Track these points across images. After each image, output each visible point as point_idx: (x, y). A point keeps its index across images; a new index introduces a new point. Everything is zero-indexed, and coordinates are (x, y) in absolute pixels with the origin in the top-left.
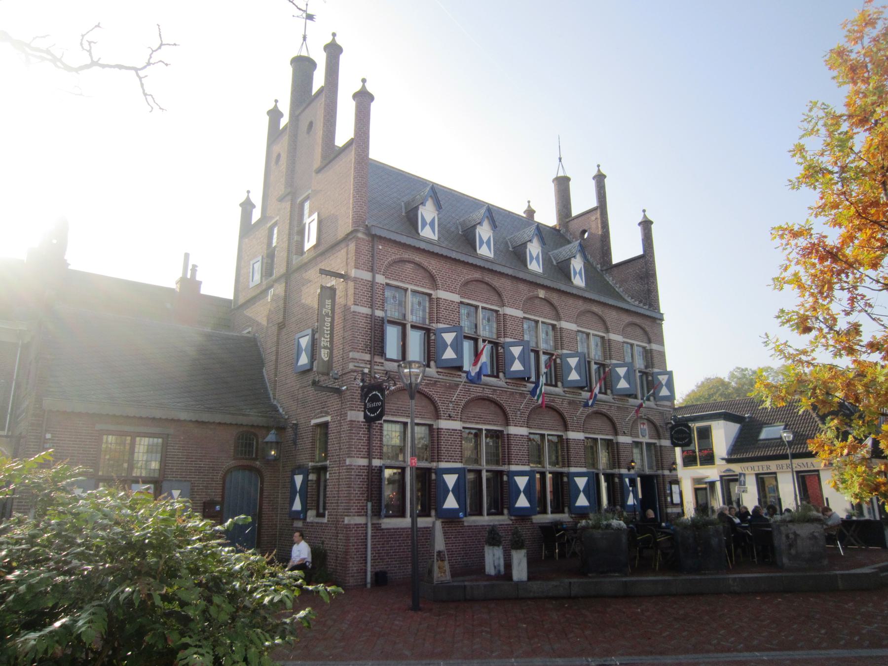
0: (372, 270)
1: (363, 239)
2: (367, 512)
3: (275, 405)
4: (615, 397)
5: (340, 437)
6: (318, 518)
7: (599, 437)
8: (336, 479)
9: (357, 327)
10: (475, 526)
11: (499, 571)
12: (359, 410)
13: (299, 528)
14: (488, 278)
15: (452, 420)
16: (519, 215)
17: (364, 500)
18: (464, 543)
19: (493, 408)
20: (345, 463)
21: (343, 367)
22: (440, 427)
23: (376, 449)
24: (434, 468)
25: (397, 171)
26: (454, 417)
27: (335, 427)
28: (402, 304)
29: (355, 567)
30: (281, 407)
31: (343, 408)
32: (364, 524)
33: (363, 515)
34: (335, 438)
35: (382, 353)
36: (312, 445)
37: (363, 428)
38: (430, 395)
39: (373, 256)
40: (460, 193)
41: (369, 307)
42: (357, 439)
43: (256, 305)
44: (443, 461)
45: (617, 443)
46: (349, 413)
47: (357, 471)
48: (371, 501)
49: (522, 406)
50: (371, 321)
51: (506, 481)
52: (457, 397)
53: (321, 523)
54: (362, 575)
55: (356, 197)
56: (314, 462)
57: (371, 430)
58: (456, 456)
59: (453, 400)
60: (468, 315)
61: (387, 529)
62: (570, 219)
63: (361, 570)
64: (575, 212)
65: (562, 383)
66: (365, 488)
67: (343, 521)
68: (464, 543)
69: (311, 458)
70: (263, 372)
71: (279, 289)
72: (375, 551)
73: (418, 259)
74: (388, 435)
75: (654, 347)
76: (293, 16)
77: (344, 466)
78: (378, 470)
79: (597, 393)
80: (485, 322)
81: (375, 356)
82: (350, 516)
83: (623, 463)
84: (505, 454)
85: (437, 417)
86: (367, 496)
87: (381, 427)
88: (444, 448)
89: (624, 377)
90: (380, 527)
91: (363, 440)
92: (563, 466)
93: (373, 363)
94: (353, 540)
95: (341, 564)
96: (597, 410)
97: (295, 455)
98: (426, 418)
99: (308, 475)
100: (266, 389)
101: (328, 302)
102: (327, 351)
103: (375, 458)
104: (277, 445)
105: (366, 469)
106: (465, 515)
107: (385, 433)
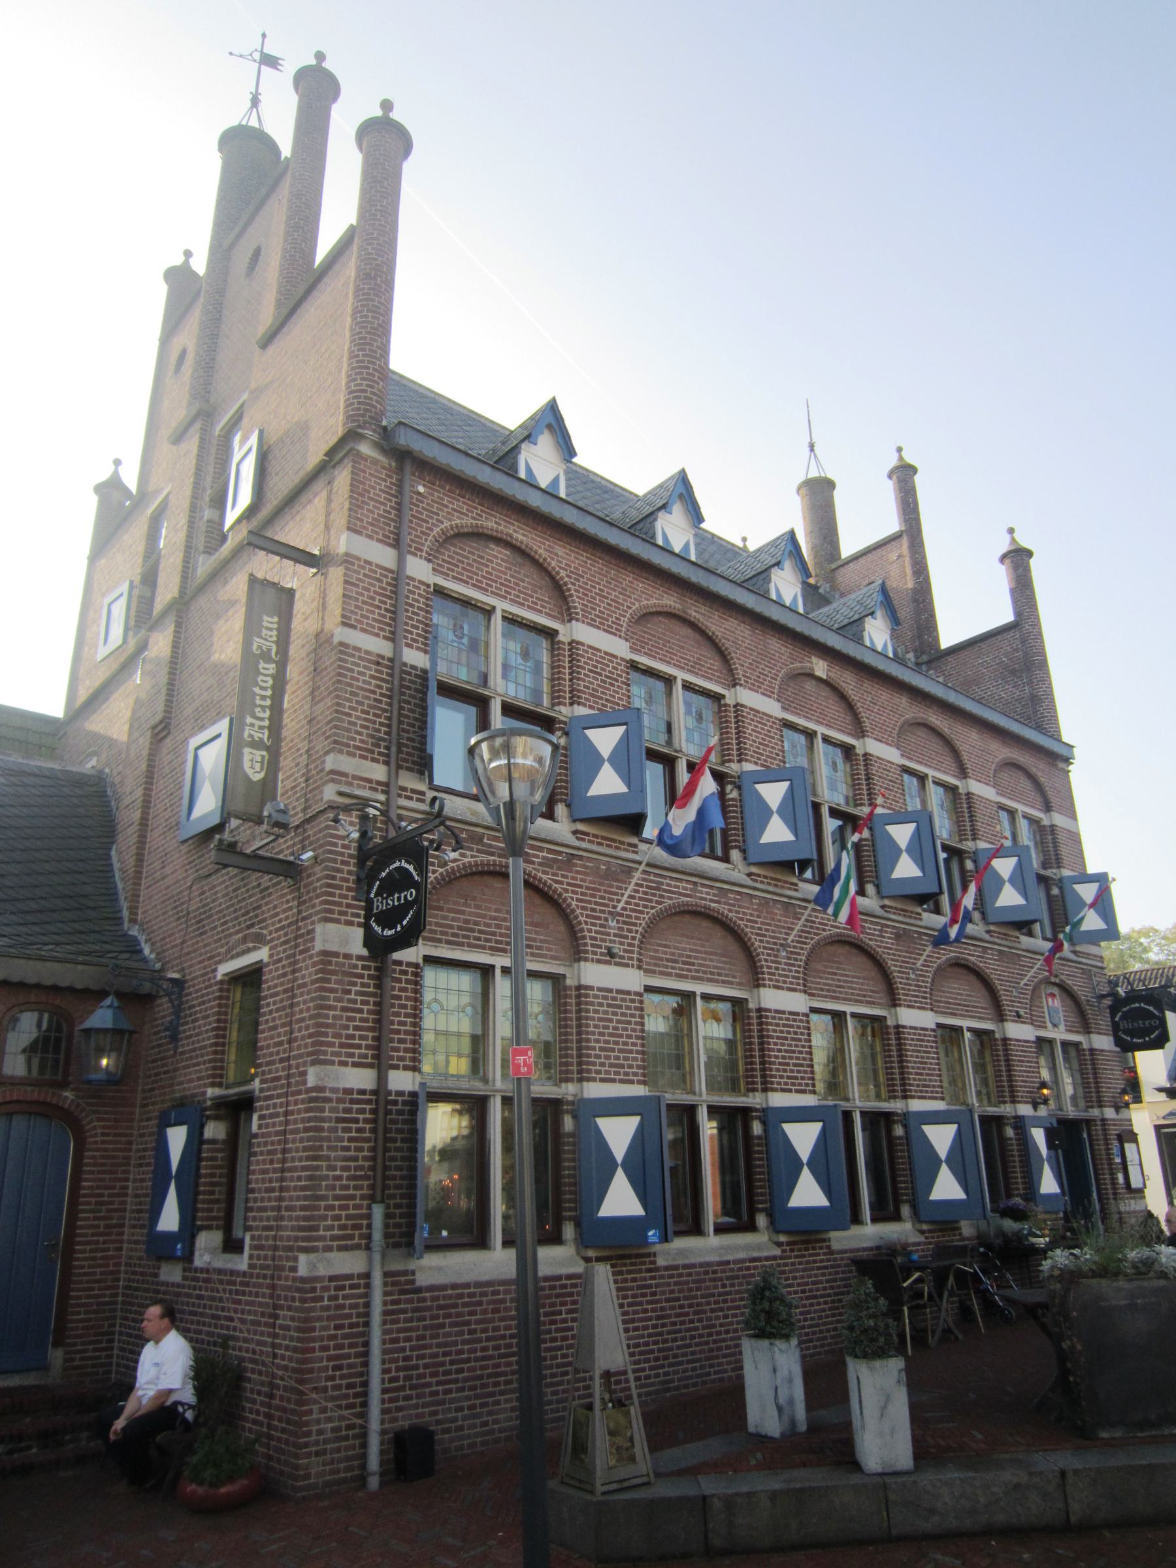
0: (396, 543)
1: (375, 462)
2: (369, 1237)
3: (135, 937)
4: (992, 928)
5: (292, 1006)
6: (228, 1256)
7: (965, 1023)
8: (277, 1133)
9: (351, 685)
10: (685, 1266)
11: (793, 1423)
12: (349, 923)
13: (173, 1285)
14: (697, 611)
15: (617, 964)
16: (733, 545)
17: (363, 1197)
18: (658, 1318)
19: (719, 938)
20: (305, 1082)
21: (307, 801)
22: (583, 982)
23: (400, 1041)
24: (570, 1098)
25: (465, 412)
26: (622, 957)
27: (279, 977)
28: (479, 647)
29: (329, 1420)
30: (146, 941)
31: (304, 919)
32: (360, 1276)
33: (357, 1247)
34: (277, 1010)
35: (423, 764)
36: (217, 1036)
37: (361, 976)
38: (555, 891)
39: (399, 508)
40: (607, 481)
41: (385, 638)
42: (344, 1009)
43: (111, 699)
44: (594, 1080)
45: (1005, 1040)
46: (319, 929)
47: (341, 1106)
48: (382, 1201)
49: (791, 938)
50: (391, 675)
51: (759, 1137)
52: (627, 903)
53: (232, 1273)
54: (353, 1447)
55: (358, 356)
56: (220, 1085)
57: (388, 983)
58: (630, 1066)
59: (619, 909)
60: (650, 700)
61: (431, 1288)
62: (839, 563)
63: (349, 1427)
64: (846, 551)
65: (877, 886)
66: (365, 1158)
67: (294, 1269)
68: (658, 1318)
69: (213, 1076)
70: (109, 857)
71: (161, 644)
72: (396, 1360)
73: (520, 537)
74: (436, 1000)
75: (1059, 819)
76: (231, 54)
77: (299, 1092)
78: (405, 1103)
79: (970, 907)
80: (691, 722)
81: (401, 772)
82: (313, 1250)
83: (1021, 1092)
84: (752, 1056)
85: (577, 954)
86: (372, 1187)
87: (416, 975)
88: (598, 1041)
89: (1012, 881)
90: (413, 1282)
91: (361, 1011)
92: (892, 1097)
93: (394, 791)
94: (323, 1329)
95: (284, 1410)
96: (958, 958)
97: (176, 1070)
98: (545, 956)
99: (202, 1126)
100: (112, 895)
101: (270, 622)
102: (259, 754)
103: (396, 1067)
104: (118, 1037)
105: (369, 1102)
106: (665, 1239)
107: (428, 996)
